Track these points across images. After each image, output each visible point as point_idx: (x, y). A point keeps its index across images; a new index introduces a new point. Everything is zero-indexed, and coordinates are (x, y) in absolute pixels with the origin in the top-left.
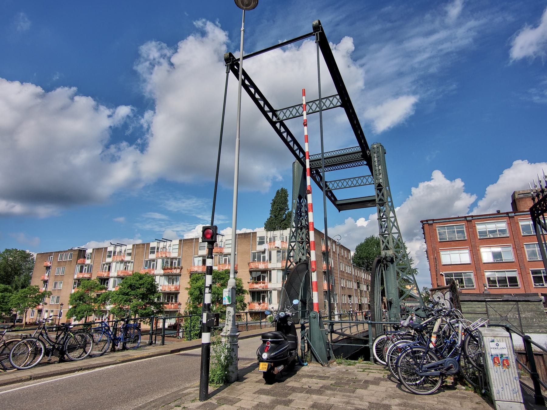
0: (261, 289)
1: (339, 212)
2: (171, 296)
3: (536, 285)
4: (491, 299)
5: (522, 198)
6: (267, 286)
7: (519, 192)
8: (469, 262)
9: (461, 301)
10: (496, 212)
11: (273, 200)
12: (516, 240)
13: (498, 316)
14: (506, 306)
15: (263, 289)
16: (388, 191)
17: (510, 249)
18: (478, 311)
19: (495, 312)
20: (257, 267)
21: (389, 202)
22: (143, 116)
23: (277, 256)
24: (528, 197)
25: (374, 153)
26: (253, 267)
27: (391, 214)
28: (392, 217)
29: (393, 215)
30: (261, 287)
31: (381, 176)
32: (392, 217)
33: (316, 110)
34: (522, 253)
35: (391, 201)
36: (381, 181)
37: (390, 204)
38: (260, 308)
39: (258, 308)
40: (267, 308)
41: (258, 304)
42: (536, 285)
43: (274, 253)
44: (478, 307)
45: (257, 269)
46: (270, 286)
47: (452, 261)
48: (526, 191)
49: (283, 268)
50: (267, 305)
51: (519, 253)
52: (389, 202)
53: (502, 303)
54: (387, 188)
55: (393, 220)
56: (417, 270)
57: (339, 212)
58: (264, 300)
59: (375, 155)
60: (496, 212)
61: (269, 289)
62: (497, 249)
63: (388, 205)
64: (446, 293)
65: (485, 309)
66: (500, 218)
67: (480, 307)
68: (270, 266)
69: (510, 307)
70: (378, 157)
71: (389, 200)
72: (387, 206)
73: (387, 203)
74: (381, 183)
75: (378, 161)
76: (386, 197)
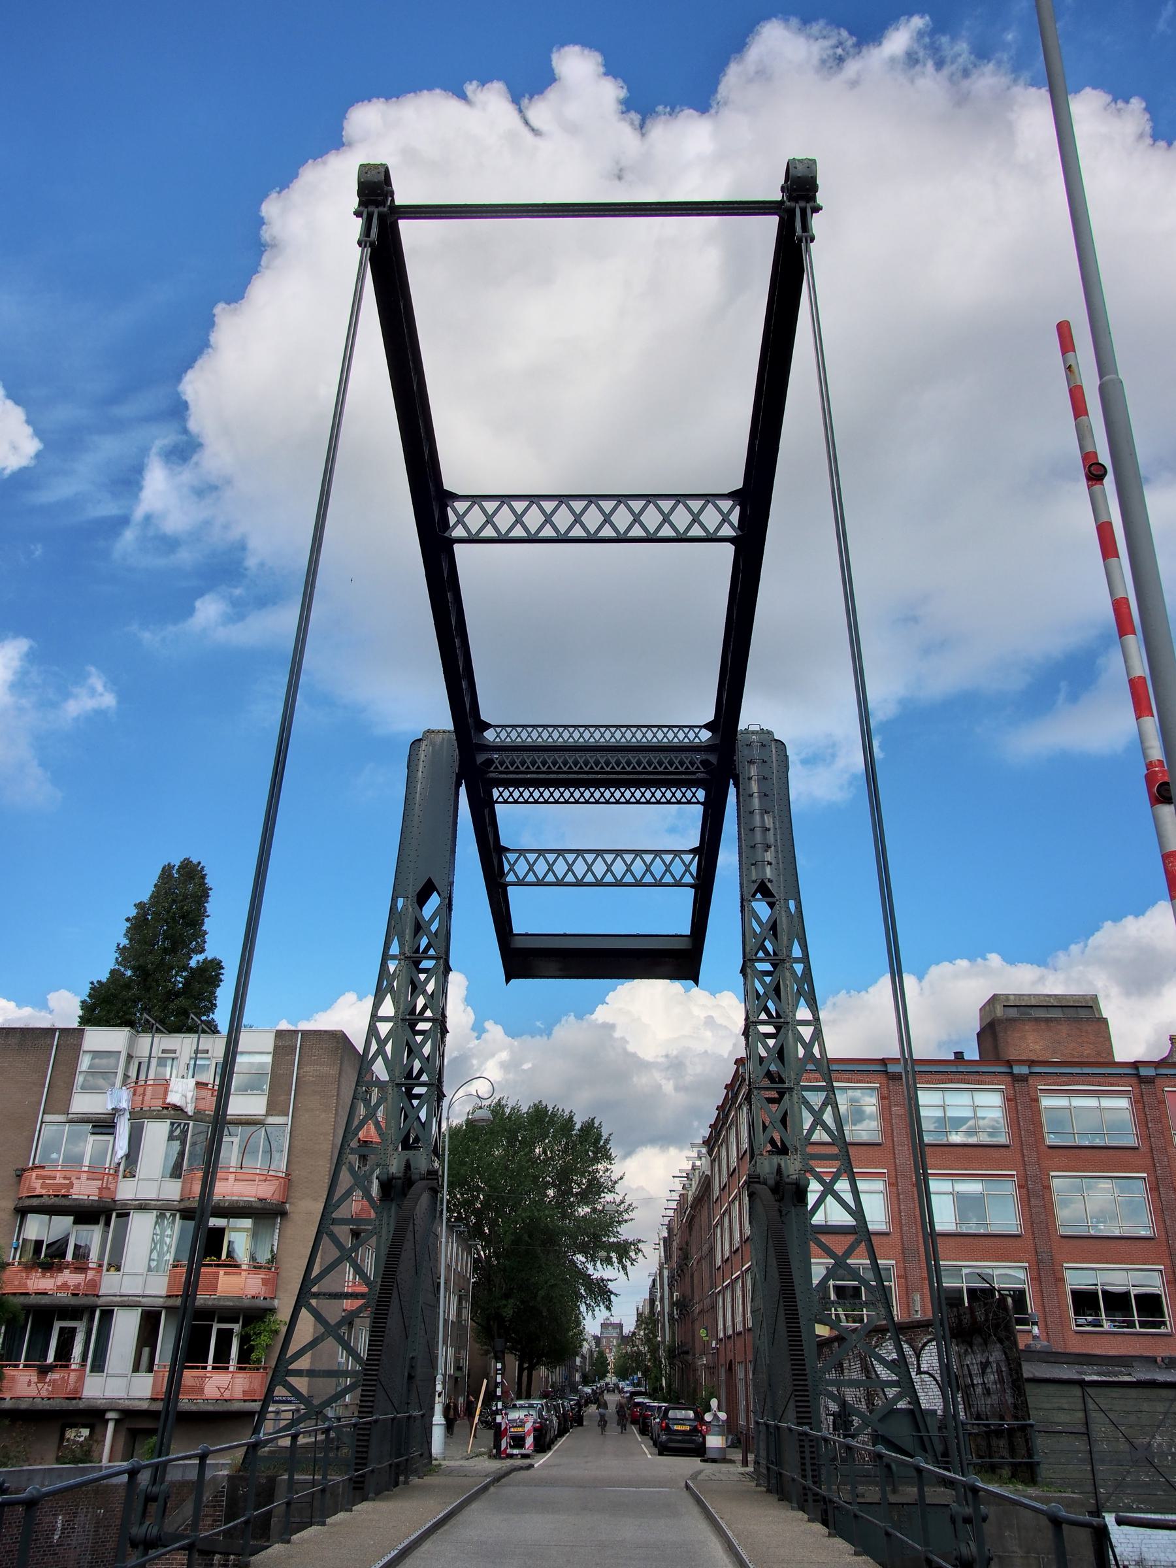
0: (63, 1297)
1: (507, 981)
2: (216, 1326)
3: (1080, 1321)
4: (1099, 1374)
5: (1012, 1020)
6: (94, 1284)
7: (1008, 1000)
8: (1014, 1230)
9: (1029, 1380)
10: (952, 1057)
11: (140, 906)
12: (1031, 1160)
13: (1123, 1446)
14: (1146, 1407)
15: (74, 1301)
16: (796, 919)
17: (1009, 1188)
18: (1059, 1424)
19: (1113, 1428)
20: (63, 1192)
21: (797, 960)
22: (608, 75)
23: (167, 1145)
24: (1030, 1020)
25: (751, 762)
26: (44, 1192)
27: (803, 1013)
28: (805, 1023)
29: (809, 1016)
30: (65, 1286)
31: (769, 856)
32: (805, 1023)
33: (630, 534)
34: (1044, 1206)
35: (805, 959)
36: (769, 872)
37: (799, 968)
38: (44, 1393)
39: (34, 1392)
40: (76, 1391)
41: (33, 1376)
42: (1080, 1321)
43: (157, 1133)
44: (1060, 1409)
45: (64, 1202)
46: (111, 1285)
47: (828, 1219)
48: (1026, 998)
49: (187, 1204)
50: (81, 1380)
51: (1035, 1206)
52: (797, 960)
53: (1133, 1393)
54: (792, 904)
55: (806, 1032)
56: (640, 1246)
57: (507, 981)
58: (64, 1353)
59: (753, 771)
60: (952, 1057)
61: (101, 1301)
62: (972, 1187)
63: (794, 973)
64: (925, 1345)
65: (1081, 1415)
66: (987, 1078)
67: (1066, 1406)
68: (126, 1191)
69: (1161, 1407)
70: (763, 779)
71: (797, 952)
72: (788, 974)
73: (787, 965)
74: (770, 881)
75: (764, 795)
76: (785, 938)
